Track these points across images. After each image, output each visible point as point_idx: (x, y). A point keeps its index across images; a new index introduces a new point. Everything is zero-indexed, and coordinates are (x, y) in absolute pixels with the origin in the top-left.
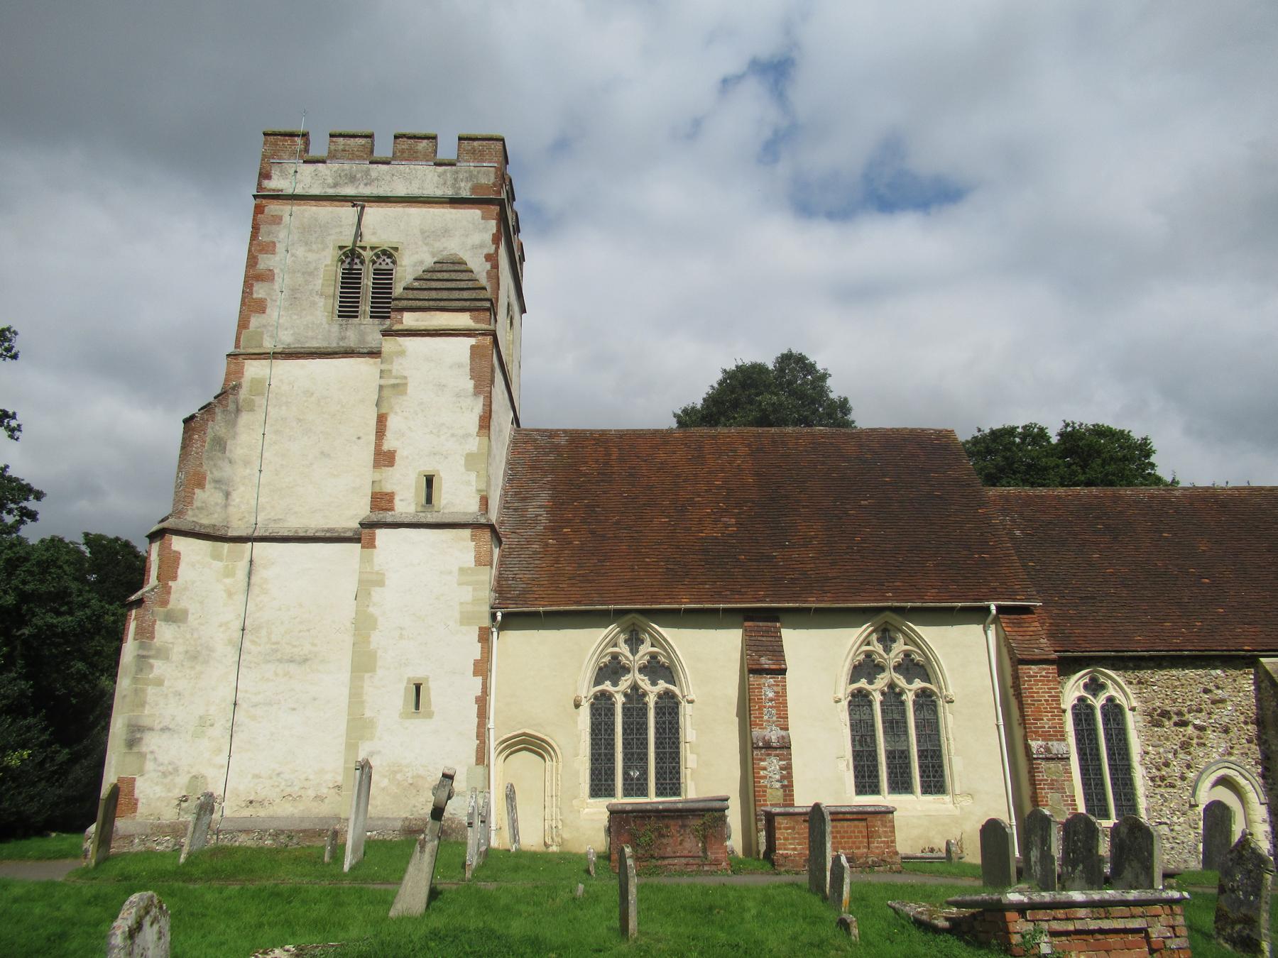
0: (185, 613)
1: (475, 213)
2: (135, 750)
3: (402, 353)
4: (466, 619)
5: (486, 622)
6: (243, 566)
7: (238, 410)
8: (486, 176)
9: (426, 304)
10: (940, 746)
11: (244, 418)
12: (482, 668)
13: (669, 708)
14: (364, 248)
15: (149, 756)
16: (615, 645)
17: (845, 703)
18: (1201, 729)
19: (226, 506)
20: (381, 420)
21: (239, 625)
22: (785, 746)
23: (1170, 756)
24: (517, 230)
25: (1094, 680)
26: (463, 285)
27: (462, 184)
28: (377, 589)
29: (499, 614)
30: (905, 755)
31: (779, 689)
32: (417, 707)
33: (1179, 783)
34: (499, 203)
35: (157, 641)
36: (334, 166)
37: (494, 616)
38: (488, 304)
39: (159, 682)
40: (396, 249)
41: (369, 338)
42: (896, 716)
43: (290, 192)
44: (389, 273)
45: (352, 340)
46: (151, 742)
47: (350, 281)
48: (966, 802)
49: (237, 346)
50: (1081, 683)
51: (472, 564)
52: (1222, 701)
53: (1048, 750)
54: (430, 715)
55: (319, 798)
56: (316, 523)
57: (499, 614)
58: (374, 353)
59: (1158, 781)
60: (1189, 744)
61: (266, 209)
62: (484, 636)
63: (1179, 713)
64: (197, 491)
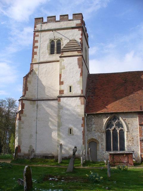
1: (77, 30)
8: (79, 22)
12: (69, 39)
20: (60, 75)
24: (86, 31)
28: (62, 110)
29: (86, 115)
34: (82, 27)
37: (85, 115)
38: (80, 49)
49: (32, 62)
57: (86, 115)
58: (58, 61)
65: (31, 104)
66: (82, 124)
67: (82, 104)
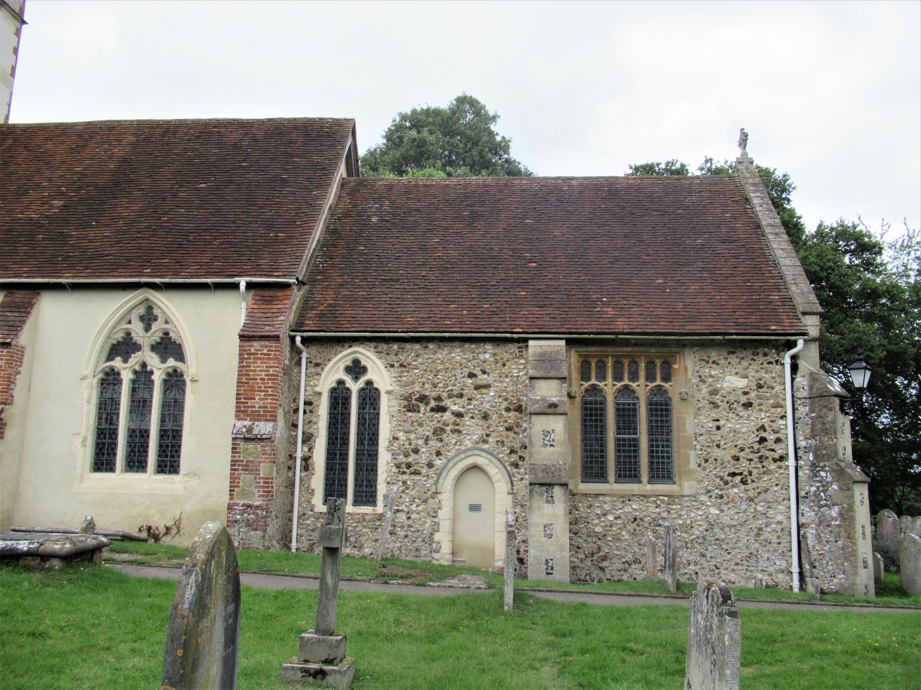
10: (181, 426)
18: (459, 415)
23: (420, 442)
30: (145, 434)
33: (424, 471)
48: (193, 483)
50: (342, 366)
52: (487, 386)
59: (405, 468)
60: (443, 430)
63: (439, 399)
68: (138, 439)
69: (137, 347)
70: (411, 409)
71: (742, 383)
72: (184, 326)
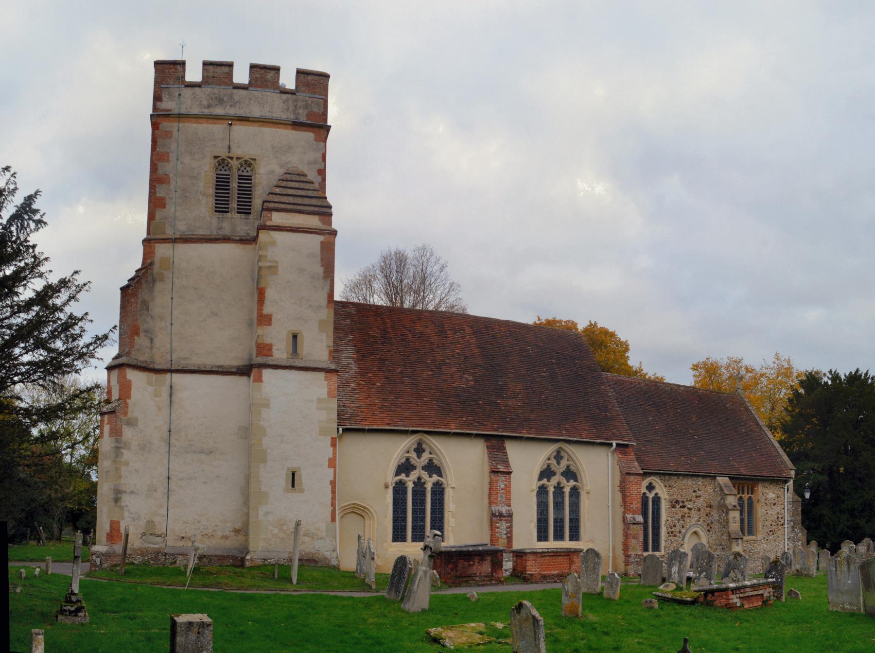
0: (136, 420)
2: (119, 504)
3: (273, 243)
4: (323, 432)
5: (335, 435)
6: (165, 390)
7: (154, 281)
9: (289, 207)
11: (159, 286)
13: (439, 491)
14: (231, 158)
15: (126, 508)
16: (408, 452)
17: (535, 492)
18: (690, 509)
19: (151, 348)
21: (166, 428)
22: (510, 516)
25: (419, 444)
26: (310, 193)
27: (301, 111)
29: (341, 429)
30: (562, 520)
31: (507, 483)
32: (293, 486)
35: (124, 438)
36: (207, 90)
39: (127, 464)
40: (255, 160)
41: (238, 229)
42: (560, 500)
43: (176, 111)
44: (249, 178)
45: (227, 230)
46: (126, 500)
47: (222, 184)
51: (326, 396)
52: (700, 496)
53: (634, 519)
54: (302, 491)
55: (225, 537)
56: (211, 361)
59: (671, 534)
61: (161, 126)
62: (333, 445)
64: (136, 338)
65: (149, 383)
66: (264, 461)
67: (330, 395)
68: (559, 523)
69: (553, 474)
70: (674, 507)
71: (773, 496)
72: (395, 456)
